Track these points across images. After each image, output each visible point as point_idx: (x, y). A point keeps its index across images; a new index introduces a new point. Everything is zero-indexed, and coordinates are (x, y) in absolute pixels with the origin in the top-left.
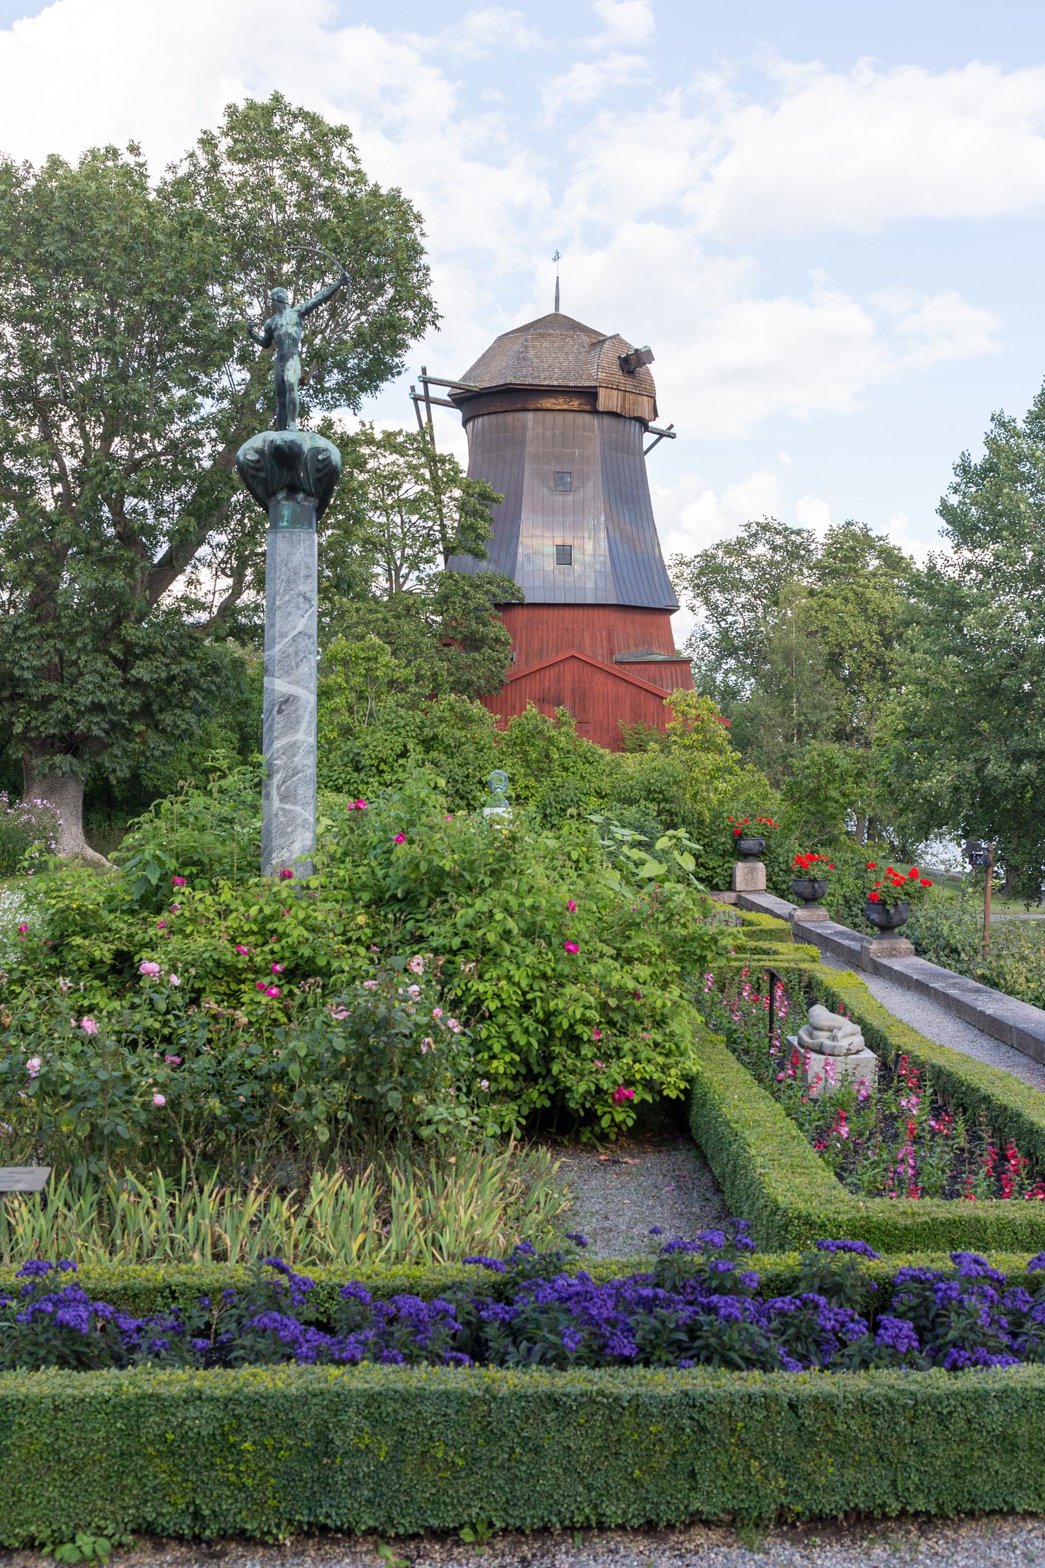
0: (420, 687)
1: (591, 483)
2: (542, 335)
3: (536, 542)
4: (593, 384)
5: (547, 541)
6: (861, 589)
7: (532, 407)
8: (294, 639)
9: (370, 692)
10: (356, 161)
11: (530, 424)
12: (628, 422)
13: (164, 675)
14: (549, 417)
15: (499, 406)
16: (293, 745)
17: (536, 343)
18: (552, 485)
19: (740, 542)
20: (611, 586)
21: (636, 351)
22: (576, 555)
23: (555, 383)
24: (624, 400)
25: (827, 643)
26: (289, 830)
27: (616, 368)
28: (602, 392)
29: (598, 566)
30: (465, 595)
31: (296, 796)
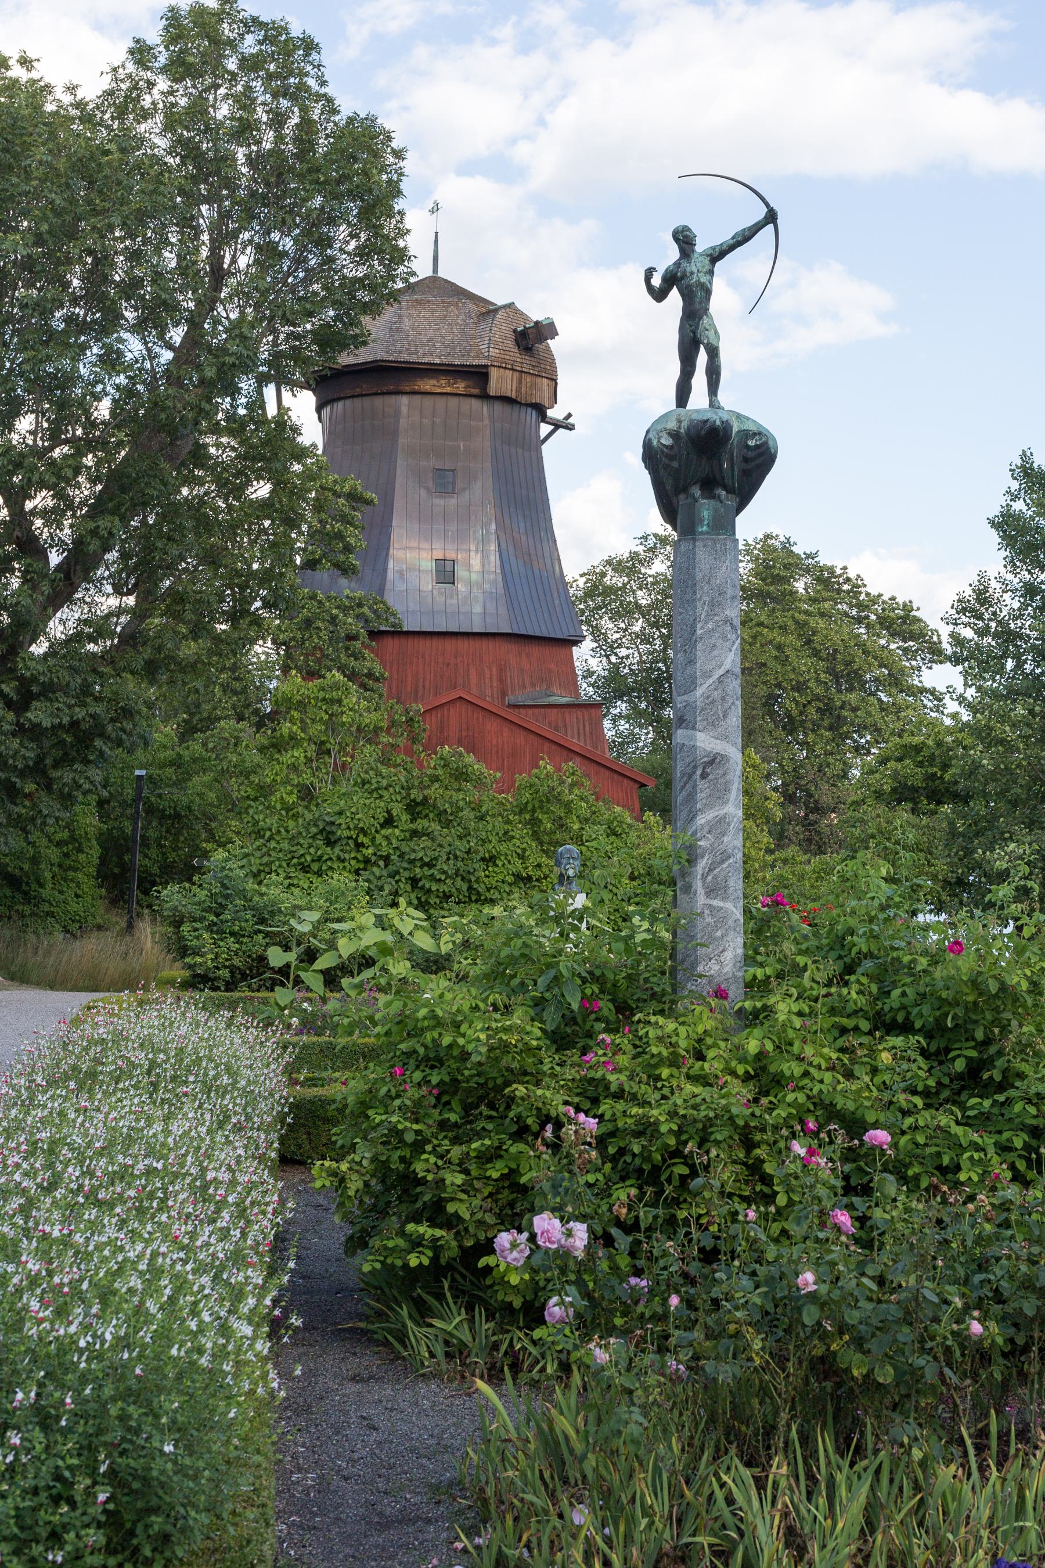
0: (394, 736)
1: (479, 484)
2: (419, 302)
3: (410, 555)
4: (484, 362)
5: (424, 555)
6: (803, 617)
7: (408, 389)
8: (720, 680)
9: (333, 745)
10: (323, 83)
11: (404, 410)
12: (523, 409)
13: (66, 720)
14: (428, 401)
15: (365, 388)
16: (721, 820)
17: (413, 312)
18: (431, 485)
19: (634, 556)
20: (503, 610)
21: (537, 323)
22: (461, 572)
23: (437, 361)
24: (520, 382)
25: (764, 683)
26: (719, 934)
27: (510, 344)
28: (494, 373)
29: (487, 586)
30: (333, 620)
31: (726, 888)
